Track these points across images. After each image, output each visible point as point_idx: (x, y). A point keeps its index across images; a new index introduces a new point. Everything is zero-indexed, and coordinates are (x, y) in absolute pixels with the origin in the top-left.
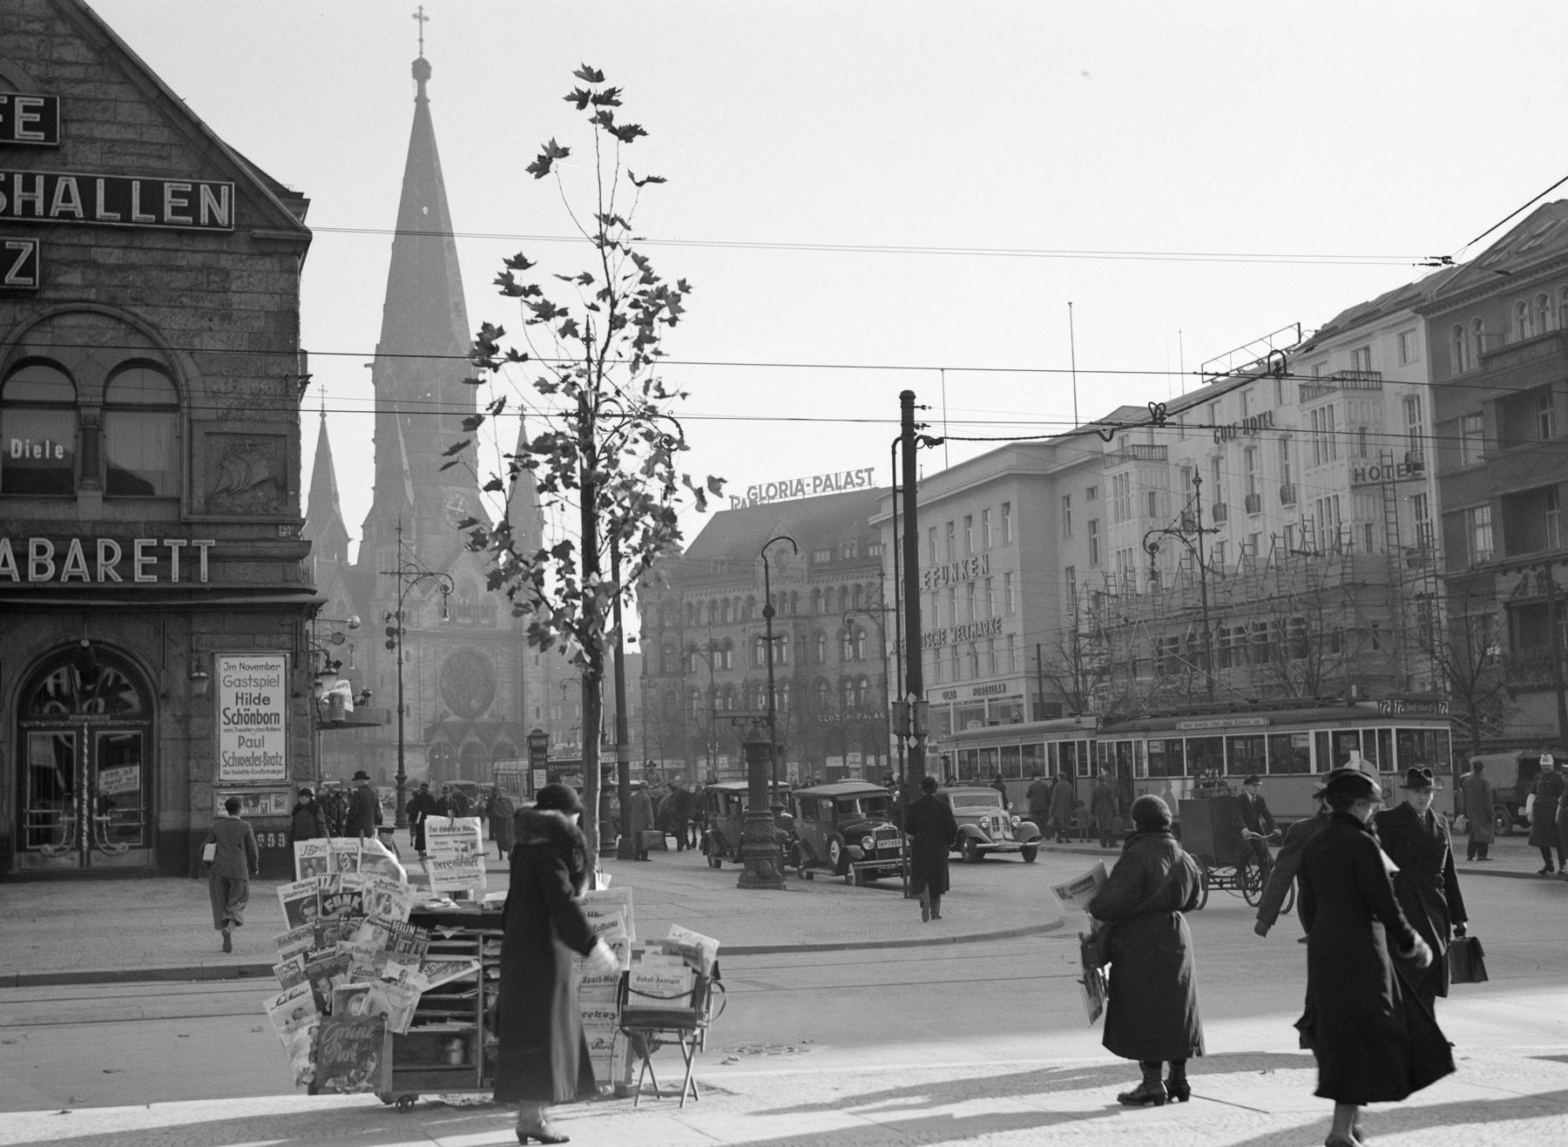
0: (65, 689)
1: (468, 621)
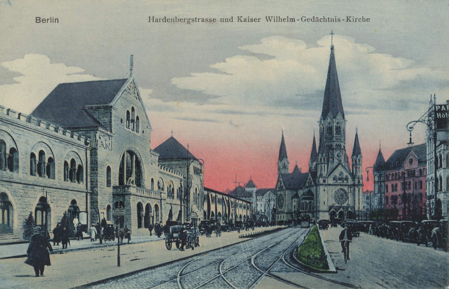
0: (86, 148)
1: (341, 181)
